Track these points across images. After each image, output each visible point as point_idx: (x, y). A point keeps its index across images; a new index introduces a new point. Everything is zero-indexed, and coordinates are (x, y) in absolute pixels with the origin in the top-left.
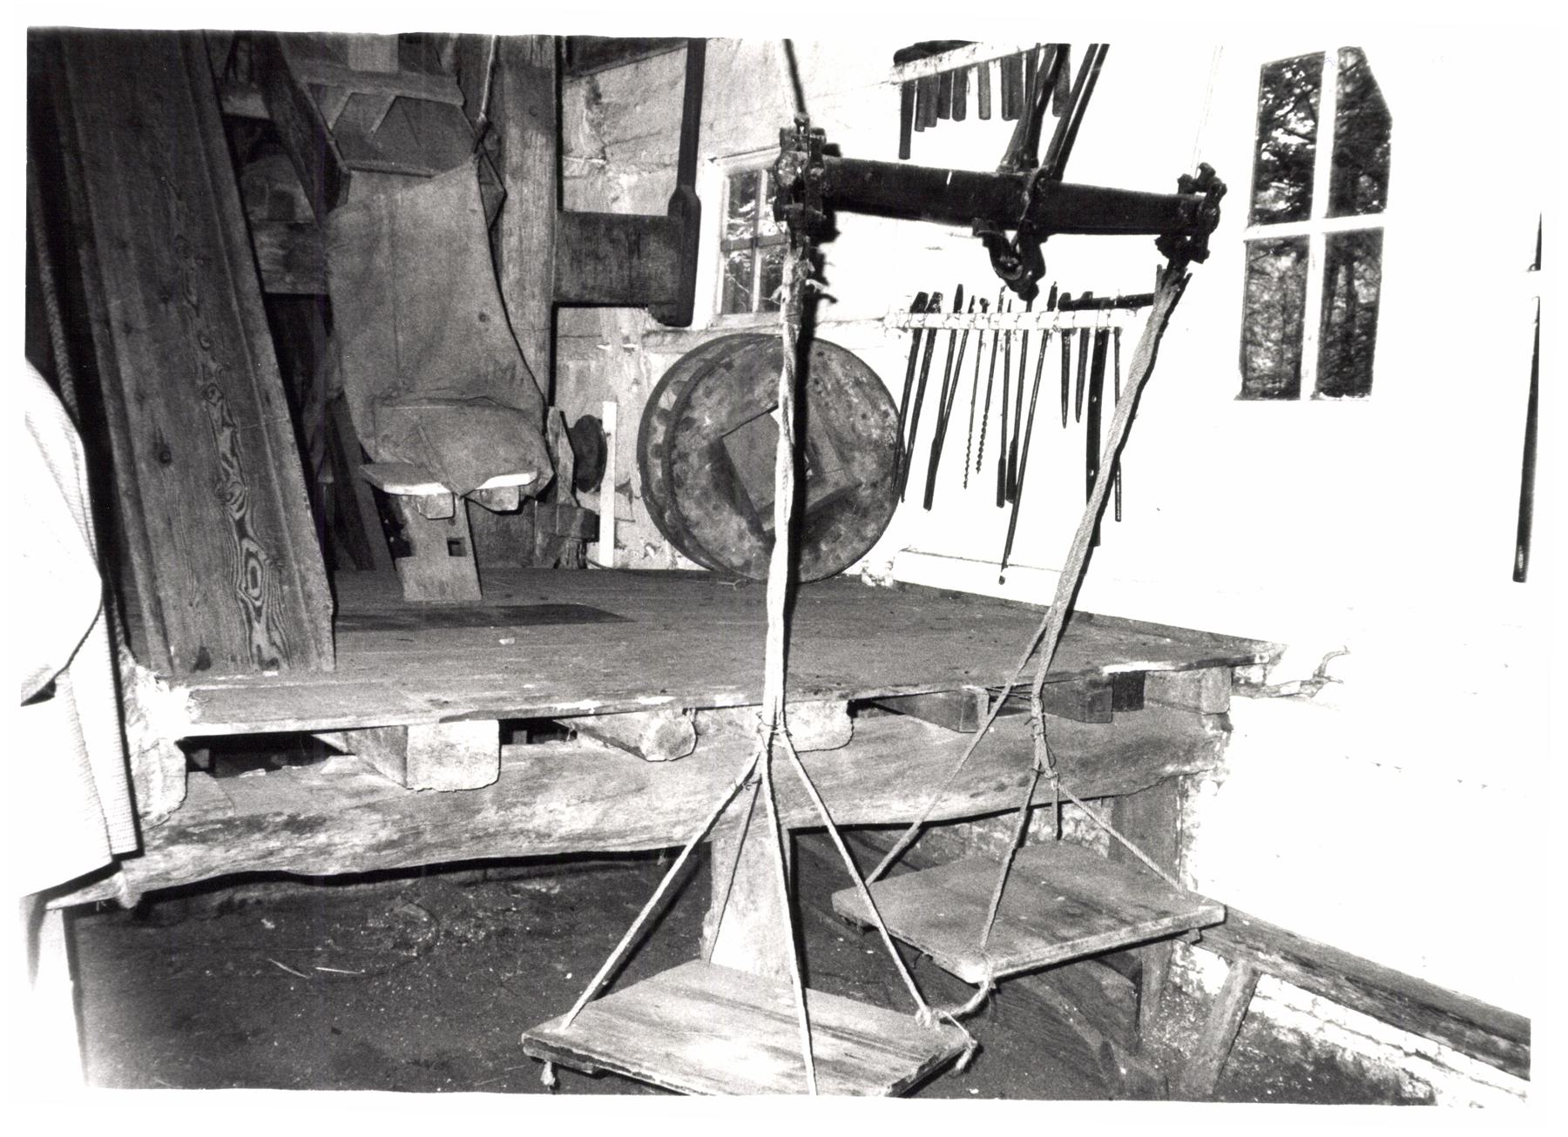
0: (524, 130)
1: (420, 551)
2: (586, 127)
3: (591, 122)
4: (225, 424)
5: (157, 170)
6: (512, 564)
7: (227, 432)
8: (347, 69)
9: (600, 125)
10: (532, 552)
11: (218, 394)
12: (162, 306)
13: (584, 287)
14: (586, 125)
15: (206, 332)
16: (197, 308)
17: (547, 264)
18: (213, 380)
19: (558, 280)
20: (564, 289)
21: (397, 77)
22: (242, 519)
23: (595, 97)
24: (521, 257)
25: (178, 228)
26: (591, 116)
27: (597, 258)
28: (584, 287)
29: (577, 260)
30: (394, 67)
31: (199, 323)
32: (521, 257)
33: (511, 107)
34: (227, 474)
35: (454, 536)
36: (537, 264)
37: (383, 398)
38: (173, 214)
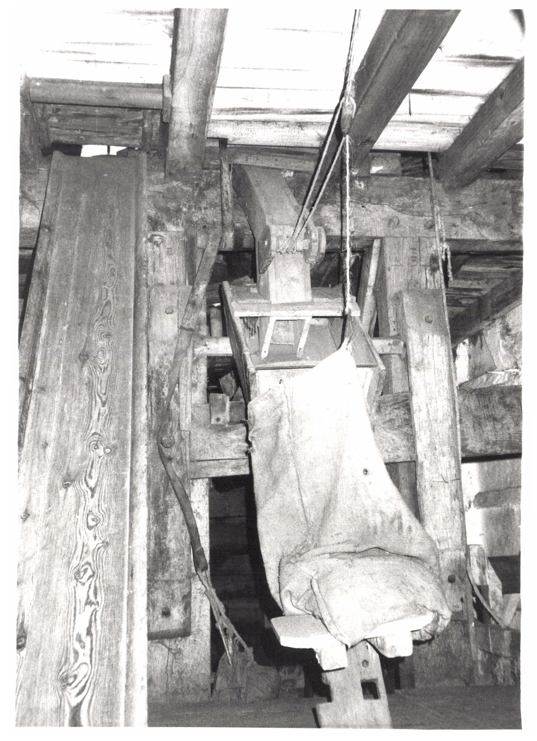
0: (421, 334)
1: (336, 695)
2: (503, 351)
3: (505, 347)
4: (89, 603)
5: (90, 385)
6: (457, 683)
7: (89, 609)
8: (270, 304)
9: (512, 347)
10: (472, 670)
11: (89, 572)
12: (62, 492)
13: (488, 443)
14: (502, 349)
15: (95, 511)
16: (93, 490)
17: (453, 426)
18: (89, 559)
19: (463, 440)
20: (469, 448)
21: (312, 303)
22: (79, 705)
23: (507, 331)
24: (430, 425)
25: (96, 426)
26: (505, 343)
27: (495, 419)
28: (488, 443)
29: (478, 422)
30: (309, 297)
31: (92, 503)
32: (430, 425)
33: (410, 319)
34: (76, 653)
35: (367, 677)
36: (444, 429)
37: (296, 555)
38: (95, 416)
